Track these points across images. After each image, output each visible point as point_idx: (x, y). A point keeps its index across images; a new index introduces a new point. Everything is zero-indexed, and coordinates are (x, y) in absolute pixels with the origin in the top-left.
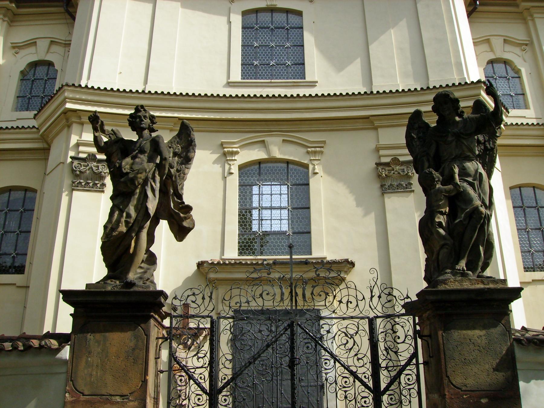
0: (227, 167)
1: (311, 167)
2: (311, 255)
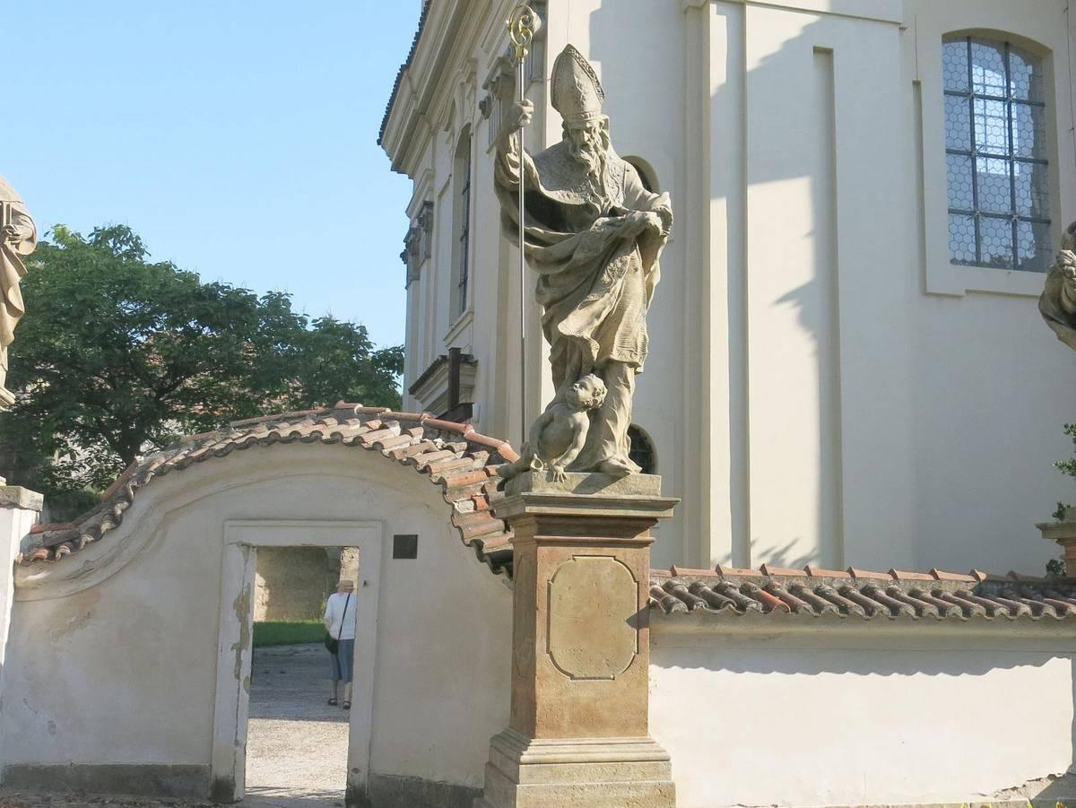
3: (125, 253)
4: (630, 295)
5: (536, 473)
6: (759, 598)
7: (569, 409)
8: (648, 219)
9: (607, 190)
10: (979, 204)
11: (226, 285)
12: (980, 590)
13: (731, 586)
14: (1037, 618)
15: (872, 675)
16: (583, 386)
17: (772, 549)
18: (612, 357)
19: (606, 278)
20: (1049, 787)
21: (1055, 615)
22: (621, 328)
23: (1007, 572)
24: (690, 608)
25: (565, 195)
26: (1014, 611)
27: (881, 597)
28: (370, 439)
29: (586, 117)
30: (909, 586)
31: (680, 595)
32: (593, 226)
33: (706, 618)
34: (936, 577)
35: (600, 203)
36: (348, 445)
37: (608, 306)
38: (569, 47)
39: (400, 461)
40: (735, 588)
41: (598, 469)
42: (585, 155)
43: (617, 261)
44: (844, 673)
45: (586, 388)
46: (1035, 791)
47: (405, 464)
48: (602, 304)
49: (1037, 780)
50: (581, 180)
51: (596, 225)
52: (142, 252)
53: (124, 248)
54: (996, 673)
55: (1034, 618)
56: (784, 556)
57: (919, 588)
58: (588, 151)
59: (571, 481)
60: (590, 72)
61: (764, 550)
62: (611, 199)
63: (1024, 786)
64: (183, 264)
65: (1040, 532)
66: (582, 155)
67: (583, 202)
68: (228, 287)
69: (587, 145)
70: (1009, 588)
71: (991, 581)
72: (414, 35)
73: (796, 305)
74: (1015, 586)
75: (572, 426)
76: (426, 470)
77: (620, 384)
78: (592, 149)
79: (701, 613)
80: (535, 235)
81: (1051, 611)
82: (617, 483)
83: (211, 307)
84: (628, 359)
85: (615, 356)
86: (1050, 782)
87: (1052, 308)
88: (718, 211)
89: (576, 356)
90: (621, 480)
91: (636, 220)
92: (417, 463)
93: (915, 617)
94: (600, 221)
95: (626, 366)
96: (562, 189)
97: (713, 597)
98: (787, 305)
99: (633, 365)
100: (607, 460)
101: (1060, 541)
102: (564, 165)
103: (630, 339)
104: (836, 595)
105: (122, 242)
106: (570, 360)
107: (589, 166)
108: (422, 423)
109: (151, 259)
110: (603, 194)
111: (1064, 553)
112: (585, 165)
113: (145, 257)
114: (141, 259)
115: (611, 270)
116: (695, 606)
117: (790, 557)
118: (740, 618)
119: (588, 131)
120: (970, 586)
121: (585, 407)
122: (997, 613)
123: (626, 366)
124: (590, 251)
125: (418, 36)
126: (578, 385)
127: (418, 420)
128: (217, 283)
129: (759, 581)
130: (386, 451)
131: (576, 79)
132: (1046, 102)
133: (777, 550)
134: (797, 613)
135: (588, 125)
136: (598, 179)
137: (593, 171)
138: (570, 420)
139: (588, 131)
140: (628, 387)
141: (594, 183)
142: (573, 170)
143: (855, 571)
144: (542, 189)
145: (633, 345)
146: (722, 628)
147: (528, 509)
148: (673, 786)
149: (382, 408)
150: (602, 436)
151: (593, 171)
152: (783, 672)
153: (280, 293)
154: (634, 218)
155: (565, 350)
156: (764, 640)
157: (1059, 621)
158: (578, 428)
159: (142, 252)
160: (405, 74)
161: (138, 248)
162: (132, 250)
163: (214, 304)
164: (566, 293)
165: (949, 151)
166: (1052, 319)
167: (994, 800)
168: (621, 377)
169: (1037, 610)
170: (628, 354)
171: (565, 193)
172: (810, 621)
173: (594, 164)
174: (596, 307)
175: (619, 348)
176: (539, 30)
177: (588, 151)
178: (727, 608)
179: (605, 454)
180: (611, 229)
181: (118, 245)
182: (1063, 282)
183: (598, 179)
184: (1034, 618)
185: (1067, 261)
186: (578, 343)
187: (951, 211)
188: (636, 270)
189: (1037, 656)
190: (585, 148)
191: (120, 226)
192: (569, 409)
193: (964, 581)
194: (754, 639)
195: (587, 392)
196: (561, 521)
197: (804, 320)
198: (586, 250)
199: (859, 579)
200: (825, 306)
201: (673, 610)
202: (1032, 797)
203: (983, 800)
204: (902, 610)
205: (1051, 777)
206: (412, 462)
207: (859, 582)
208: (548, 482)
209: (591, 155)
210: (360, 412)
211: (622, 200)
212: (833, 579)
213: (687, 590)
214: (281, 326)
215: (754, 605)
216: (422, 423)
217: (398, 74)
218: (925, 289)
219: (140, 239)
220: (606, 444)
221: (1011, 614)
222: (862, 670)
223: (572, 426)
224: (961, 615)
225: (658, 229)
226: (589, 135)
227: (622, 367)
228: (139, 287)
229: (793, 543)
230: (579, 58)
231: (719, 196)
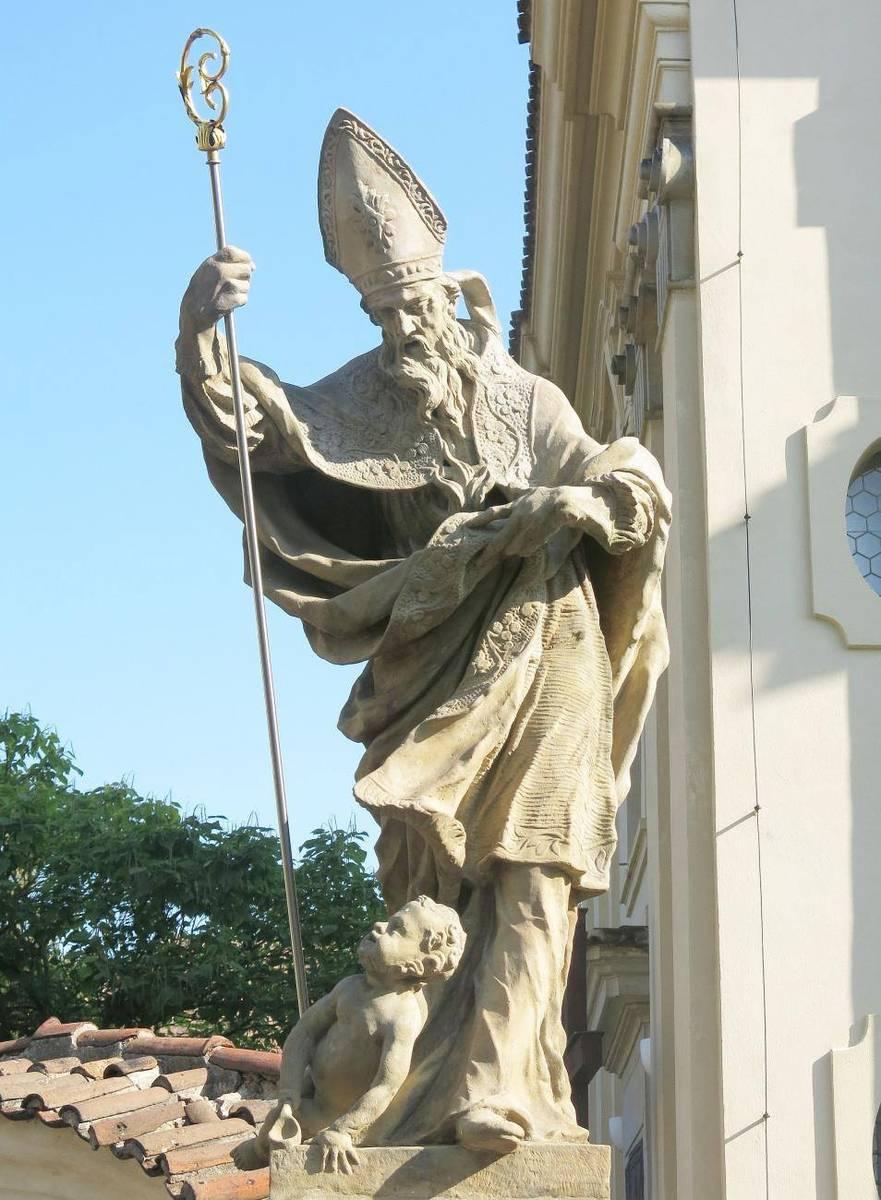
3: (34, 771)
4: (560, 698)
5: (279, 1152)
7: (369, 987)
8: (563, 504)
9: (483, 447)
11: (211, 821)
16: (397, 927)
18: (500, 853)
19: (483, 661)
22: (529, 781)
25: (379, 469)
28: (55, 1101)
29: (400, 275)
32: (437, 536)
35: (461, 479)
36: (13, 1116)
37: (495, 729)
38: (341, 117)
39: (112, 1146)
41: (449, 1135)
42: (414, 369)
43: (511, 616)
45: (403, 933)
47: (122, 1155)
48: (478, 724)
50: (419, 429)
51: (444, 532)
52: (66, 767)
53: (30, 761)
58: (422, 357)
59: (370, 1169)
60: (397, 168)
62: (490, 468)
64: (149, 788)
66: (406, 369)
67: (422, 481)
68: (216, 826)
69: (417, 343)
72: (522, 246)
75: (372, 1029)
76: (160, 1168)
77: (521, 919)
78: (433, 352)
80: (315, 572)
82: (492, 1168)
83: (179, 869)
84: (545, 857)
85: (509, 848)
89: (425, 860)
90: (503, 1161)
91: (535, 509)
92: (143, 1151)
94: (453, 522)
95: (537, 873)
96: (373, 456)
99: (555, 869)
100: (466, 1112)
102: (376, 400)
103: (552, 808)
105: (23, 750)
106: (415, 873)
107: (426, 393)
108: (206, 1059)
109: (86, 780)
110: (474, 458)
112: (416, 392)
113: (71, 776)
114: (65, 780)
115: (498, 640)
119: (413, 308)
121: (409, 981)
123: (537, 873)
124: (433, 595)
125: (529, 244)
126: (384, 926)
127: (200, 1053)
128: (194, 817)
130: (84, 1128)
131: (363, 189)
135: (407, 295)
136: (459, 424)
137: (442, 405)
138: (369, 1015)
139: (413, 308)
140: (542, 925)
141: (450, 433)
142: (395, 407)
144: (316, 459)
145: (559, 820)
149: (132, 1031)
150: (473, 1050)
151: (442, 405)
153: (340, 833)
154: (530, 505)
155: (404, 847)
158: (384, 1037)
159: (66, 767)
160: (523, 331)
161: (56, 762)
162: (44, 764)
163: (187, 864)
164: (397, 706)
168: (526, 901)
170: (542, 843)
171: (376, 464)
173: (440, 388)
174: (462, 733)
175: (520, 830)
176: (676, 180)
177: (422, 357)
179: (467, 1097)
180: (481, 536)
181: (18, 757)
183: (459, 424)
186: (408, 820)
188: (579, 636)
190: (414, 350)
191: (15, 716)
192: (369, 987)
195: (406, 942)
198: (421, 597)
206: (132, 1150)
208: (311, 1172)
209: (430, 366)
210: (85, 1042)
211: (526, 468)
214: (339, 902)
216: (206, 1059)
217: (512, 334)
219: (58, 741)
220: (474, 1072)
223: (372, 1029)
225: (599, 527)
226: (417, 319)
227: (529, 876)
228: (39, 838)
230: (368, 140)
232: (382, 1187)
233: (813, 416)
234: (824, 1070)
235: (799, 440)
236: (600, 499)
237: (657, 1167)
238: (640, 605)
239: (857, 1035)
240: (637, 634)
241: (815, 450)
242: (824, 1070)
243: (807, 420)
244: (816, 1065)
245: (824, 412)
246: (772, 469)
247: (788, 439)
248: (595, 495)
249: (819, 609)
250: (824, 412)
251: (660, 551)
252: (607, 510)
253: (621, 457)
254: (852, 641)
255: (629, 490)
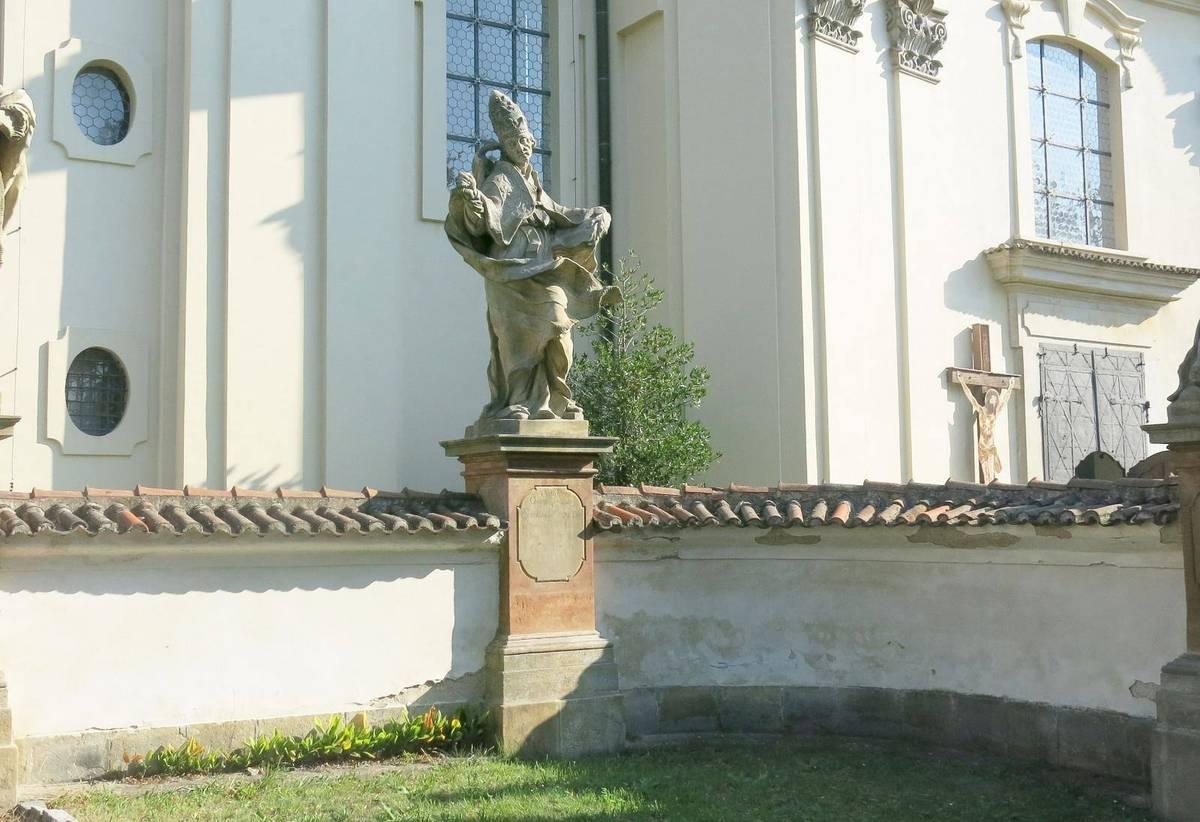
0: (1011, 39)
1: (1122, 70)
2: (1126, 249)
6: (308, 519)
10: (481, 132)
12: (368, 508)
13: (94, 507)
14: (414, 532)
15: (245, 592)
17: (255, 474)
20: (426, 694)
21: (432, 529)
23: (401, 490)
24: (34, 529)
26: (390, 525)
27: (204, 517)
30: (294, 504)
31: (330, 517)
33: (55, 541)
34: (324, 495)
40: (98, 509)
44: (290, 589)
46: (412, 698)
49: (415, 687)
54: (377, 586)
55: (411, 532)
56: (264, 483)
57: (304, 506)
61: (243, 477)
63: (401, 693)
65: (443, 449)
70: (398, 504)
71: (381, 497)
73: (286, 225)
74: (411, 503)
79: (46, 533)
81: (427, 524)
86: (428, 688)
87: (457, 231)
88: (198, 125)
93: (285, 533)
97: (339, 519)
98: (275, 225)
101: (462, 459)
104: (211, 515)
111: (464, 470)
116: (40, 528)
117: (272, 484)
118: (95, 538)
120: (359, 503)
122: (372, 528)
129: (130, 502)
132: (550, 33)
133: (256, 477)
134: (156, 532)
143: (369, 490)
146: (75, 550)
147: (503, 449)
148: (8, 712)
152: (327, 588)
156: (125, 561)
157: (435, 534)
165: (450, 76)
166: (457, 241)
167: (369, 708)
169: (413, 524)
172: (174, 540)
178: (76, 529)
182: (463, 204)
184: (411, 532)
185: (465, 184)
187: (450, 137)
189: (419, 567)
193: (353, 498)
194: (113, 560)
196: (521, 456)
197: (292, 242)
199: (241, 497)
200: (314, 227)
201: (13, 533)
202: (409, 704)
203: (357, 709)
204: (272, 527)
205: (429, 683)
207: (240, 501)
212: (212, 498)
213: (43, 514)
215: (108, 526)
218: (421, 215)
221: (312, 530)
222: (209, 587)
224: (334, 530)
229: (275, 468)
231: (199, 108)
232: (503, 212)
233: (59, 46)
234: (45, 350)
235: (51, 57)
236: (8, 117)
237: (586, 195)
238: (17, 161)
239: (61, 334)
240: (15, 173)
241: (59, 62)
242: (45, 350)
243: (55, 46)
244: (41, 347)
245: (64, 44)
246: (38, 69)
247: (46, 55)
248: (6, 114)
249: (55, 139)
250: (64, 44)
251: (29, 139)
252: (11, 122)
253: (18, 98)
254: (70, 155)
255: (21, 114)
